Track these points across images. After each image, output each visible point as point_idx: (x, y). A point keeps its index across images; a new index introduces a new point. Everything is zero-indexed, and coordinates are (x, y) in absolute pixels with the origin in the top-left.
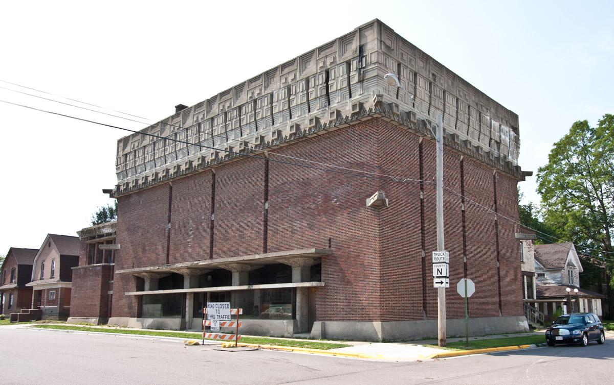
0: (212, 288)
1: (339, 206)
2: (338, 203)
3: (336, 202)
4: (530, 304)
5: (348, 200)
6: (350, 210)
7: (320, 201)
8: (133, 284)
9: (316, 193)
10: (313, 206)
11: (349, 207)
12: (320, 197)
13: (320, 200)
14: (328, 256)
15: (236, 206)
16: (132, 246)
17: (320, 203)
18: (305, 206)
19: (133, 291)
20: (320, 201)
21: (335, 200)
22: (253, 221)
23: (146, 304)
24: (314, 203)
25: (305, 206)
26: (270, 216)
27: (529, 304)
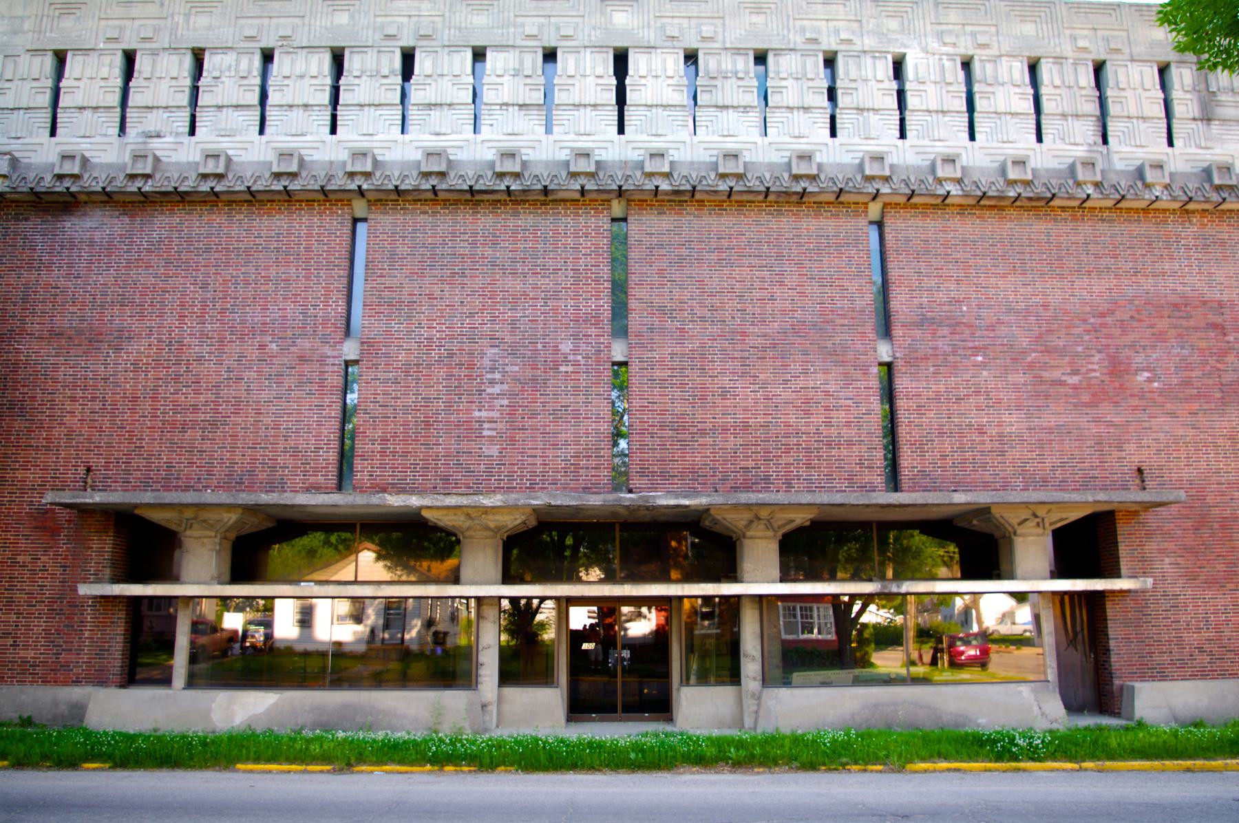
0: (703, 585)
1: (1161, 392)
2: (1156, 384)
3: (1149, 380)
4: (703, 601)
5: (1187, 383)
6: (1195, 406)
7: (1094, 370)
8: (102, 547)
9: (1080, 349)
10: (1075, 380)
11: (1189, 399)
12: (1096, 359)
13: (1096, 367)
14: (1135, 512)
15: (743, 334)
16: (430, 339)
17: (1097, 374)
18: (1045, 374)
19: (98, 581)
20: (1094, 370)
21: (1146, 374)
22: (832, 388)
23: (686, 681)
24: (1075, 372)
25: (1045, 374)
26: (902, 383)
27: (700, 601)
